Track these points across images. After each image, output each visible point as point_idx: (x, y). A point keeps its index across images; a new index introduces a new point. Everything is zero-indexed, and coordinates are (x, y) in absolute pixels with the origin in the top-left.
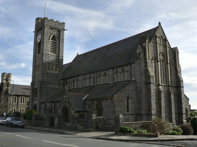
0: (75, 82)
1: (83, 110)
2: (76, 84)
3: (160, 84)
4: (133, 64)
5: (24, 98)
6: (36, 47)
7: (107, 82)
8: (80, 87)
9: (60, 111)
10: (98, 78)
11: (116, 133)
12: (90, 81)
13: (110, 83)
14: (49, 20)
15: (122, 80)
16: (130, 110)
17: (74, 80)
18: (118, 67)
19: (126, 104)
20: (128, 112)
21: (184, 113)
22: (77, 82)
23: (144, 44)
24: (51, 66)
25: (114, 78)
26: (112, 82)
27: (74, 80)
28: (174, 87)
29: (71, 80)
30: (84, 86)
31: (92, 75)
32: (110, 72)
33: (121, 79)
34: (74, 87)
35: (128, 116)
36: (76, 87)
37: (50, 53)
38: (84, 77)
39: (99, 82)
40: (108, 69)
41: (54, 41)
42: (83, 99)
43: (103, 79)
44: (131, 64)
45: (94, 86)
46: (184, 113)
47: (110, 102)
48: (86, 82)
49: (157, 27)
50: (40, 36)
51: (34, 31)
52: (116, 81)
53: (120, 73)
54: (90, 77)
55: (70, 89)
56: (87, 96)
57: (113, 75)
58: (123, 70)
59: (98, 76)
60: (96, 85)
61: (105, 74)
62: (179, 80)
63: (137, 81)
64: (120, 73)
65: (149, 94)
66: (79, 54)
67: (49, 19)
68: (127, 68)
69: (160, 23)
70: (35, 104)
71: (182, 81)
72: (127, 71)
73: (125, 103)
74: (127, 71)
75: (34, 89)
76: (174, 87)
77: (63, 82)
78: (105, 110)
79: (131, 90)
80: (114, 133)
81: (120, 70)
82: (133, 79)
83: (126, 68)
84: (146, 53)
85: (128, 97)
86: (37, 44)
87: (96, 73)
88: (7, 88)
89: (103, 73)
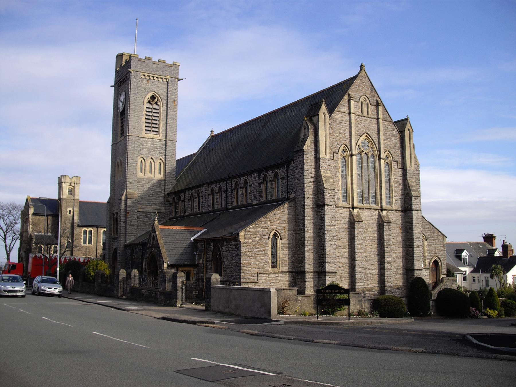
0: (195, 200)
1: (186, 263)
2: (196, 205)
3: (356, 204)
4: (292, 162)
5: (90, 232)
6: (117, 119)
7: (249, 201)
8: (204, 211)
9: (145, 265)
10: (235, 192)
11: (207, 310)
12: (221, 196)
13: (254, 203)
14: (140, 60)
15: (274, 198)
16: (280, 262)
17: (192, 195)
18: (267, 169)
19: (270, 250)
20: (274, 266)
21: (309, 273)
22: (197, 199)
23: (314, 119)
24: (148, 164)
25: (260, 192)
26: (258, 202)
27: (192, 195)
28: (396, 210)
29: (188, 194)
30: (211, 208)
31: (223, 185)
32: (254, 179)
33: (272, 196)
34: (199, 209)
35: (273, 276)
36: (196, 210)
37: (144, 134)
38: (262, 176)
39: (235, 200)
40: (251, 173)
41: (155, 106)
42: (192, 239)
43: (242, 193)
44: (289, 163)
45: (227, 209)
46: (309, 273)
47: (234, 247)
48: (213, 199)
49: (356, 75)
50: (122, 98)
51: (113, 84)
52: (264, 199)
53: (270, 181)
54: (220, 188)
55: (186, 214)
56: (201, 232)
57: (260, 187)
58: (276, 175)
59: (233, 187)
60: (230, 207)
61: (246, 182)
62: (409, 193)
63: (297, 200)
64: (270, 181)
65: (322, 228)
66: (215, 133)
67: (142, 56)
68: (282, 172)
69: (362, 67)
70: (115, 248)
71: (418, 197)
72: (283, 179)
73: (267, 248)
74: (283, 179)
75: (113, 214)
76: (396, 210)
77: (174, 199)
78: (226, 262)
79: (283, 219)
80: (204, 308)
81: (270, 174)
82: (292, 196)
83: (281, 171)
84: (318, 140)
85: (275, 235)
86: (119, 115)
87: (230, 180)
88: (72, 211)
89: (242, 180)
